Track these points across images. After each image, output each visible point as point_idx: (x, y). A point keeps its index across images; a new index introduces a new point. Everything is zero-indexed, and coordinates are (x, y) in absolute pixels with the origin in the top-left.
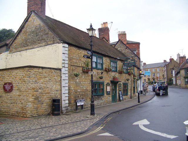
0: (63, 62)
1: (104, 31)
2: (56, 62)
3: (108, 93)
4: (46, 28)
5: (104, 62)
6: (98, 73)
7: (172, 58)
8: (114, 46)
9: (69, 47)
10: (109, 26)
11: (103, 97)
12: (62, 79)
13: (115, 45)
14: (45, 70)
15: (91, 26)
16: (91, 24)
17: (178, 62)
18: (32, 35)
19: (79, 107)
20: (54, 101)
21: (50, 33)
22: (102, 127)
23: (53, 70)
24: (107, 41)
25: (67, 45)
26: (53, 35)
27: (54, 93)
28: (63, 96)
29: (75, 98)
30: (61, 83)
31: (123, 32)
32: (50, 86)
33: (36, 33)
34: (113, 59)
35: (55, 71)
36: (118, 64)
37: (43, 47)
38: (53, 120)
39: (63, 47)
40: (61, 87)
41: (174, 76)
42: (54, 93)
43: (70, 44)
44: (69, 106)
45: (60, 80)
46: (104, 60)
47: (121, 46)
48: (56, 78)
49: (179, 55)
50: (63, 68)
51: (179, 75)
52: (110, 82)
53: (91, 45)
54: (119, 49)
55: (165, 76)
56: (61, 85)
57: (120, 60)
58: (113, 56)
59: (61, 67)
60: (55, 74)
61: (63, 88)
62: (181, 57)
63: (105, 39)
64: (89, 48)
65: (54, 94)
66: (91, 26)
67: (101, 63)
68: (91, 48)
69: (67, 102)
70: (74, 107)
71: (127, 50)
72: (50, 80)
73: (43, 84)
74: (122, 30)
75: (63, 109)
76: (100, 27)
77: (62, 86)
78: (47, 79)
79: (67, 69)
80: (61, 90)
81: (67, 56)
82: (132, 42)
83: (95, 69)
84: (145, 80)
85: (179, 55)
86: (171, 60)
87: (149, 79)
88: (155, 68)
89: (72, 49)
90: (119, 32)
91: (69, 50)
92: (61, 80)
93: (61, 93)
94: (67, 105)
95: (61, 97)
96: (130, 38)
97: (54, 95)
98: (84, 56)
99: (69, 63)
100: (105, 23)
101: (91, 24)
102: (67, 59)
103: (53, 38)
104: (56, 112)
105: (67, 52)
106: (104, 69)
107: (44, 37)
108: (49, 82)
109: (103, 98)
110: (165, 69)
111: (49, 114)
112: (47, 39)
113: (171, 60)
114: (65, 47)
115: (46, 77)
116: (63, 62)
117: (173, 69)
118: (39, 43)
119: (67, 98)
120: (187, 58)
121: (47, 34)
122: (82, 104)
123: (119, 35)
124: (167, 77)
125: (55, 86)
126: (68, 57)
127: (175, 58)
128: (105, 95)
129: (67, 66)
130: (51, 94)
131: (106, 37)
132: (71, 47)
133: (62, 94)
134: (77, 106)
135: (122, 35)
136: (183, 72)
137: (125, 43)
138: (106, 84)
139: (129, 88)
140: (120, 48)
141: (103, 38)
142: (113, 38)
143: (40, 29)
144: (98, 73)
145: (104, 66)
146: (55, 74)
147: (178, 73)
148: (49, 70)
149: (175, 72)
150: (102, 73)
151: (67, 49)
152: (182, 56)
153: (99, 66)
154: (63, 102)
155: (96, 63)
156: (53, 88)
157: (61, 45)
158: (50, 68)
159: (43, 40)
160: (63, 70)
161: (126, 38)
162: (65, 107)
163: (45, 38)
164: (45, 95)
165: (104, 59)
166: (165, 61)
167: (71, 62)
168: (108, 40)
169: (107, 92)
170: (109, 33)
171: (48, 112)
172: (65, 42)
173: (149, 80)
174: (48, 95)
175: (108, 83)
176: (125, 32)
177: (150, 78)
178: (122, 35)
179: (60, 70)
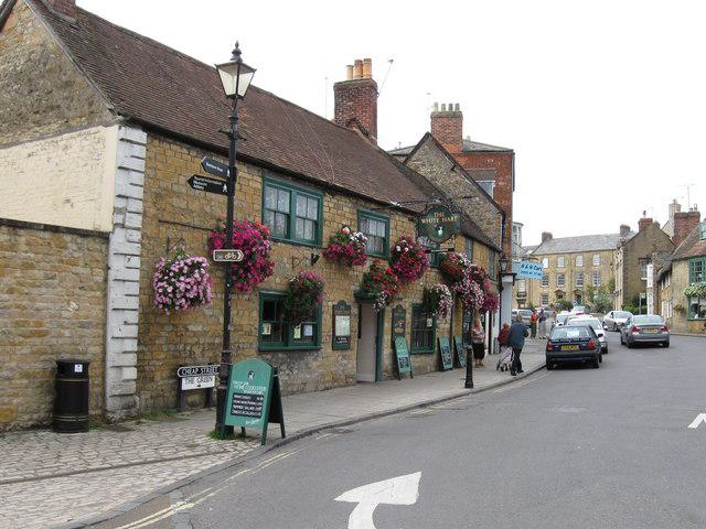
0: (121, 203)
1: (357, 94)
2: (93, 203)
3: (340, 344)
4: (68, 59)
5: (326, 215)
6: (293, 258)
7: (648, 216)
8: (402, 159)
9: (156, 142)
10: (377, 74)
11: (315, 359)
12: (112, 274)
13: (408, 157)
14: (24, 237)
15: (237, 53)
16: (237, 45)
17: (671, 234)
18: (15, 87)
19: (191, 399)
20: (64, 368)
21: (79, 79)
22: (191, 505)
23: (67, 238)
24: (367, 135)
25: (139, 135)
26: (90, 91)
27: (67, 333)
28: (113, 348)
29: (175, 357)
30: (105, 296)
31: (451, 106)
32: (50, 305)
33: (29, 80)
34: (373, 206)
35: (79, 240)
36: (392, 226)
37: (49, 140)
38: (73, 449)
39: (122, 140)
40: (105, 312)
41: (650, 283)
42: (67, 333)
43: (154, 131)
44: (138, 393)
45: (100, 279)
46: (325, 209)
47: (433, 159)
48: (80, 270)
49: (675, 205)
50: (118, 230)
51: (668, 283)
52: (353, 299)
53: (231, 136)
54: (423, 171)
55: (619, 286)
56: (105, 303)
57: (405, 212)
58: (371, 194)
59: (106, 227)
60: (76, 255)
61: (111, 314)
62: (684, 214)
63: (360, 128)
64: (225, 143)
65: (68, 341)
66: (237, 53)
67: (287, 211)
68: (233, 145)
69: (131, 373)
70: (171, 397)
71: (457, 177)
72: (53, 278)
73: (15, 296)
74: (446, 99)
75: (111, 404)
76: (343, 77)
77: (111, 306)
78: (38, 274)
79: (137, 236)
80: (105, 325)
81: (138, 178)
82: (490, 149)
83: (285, 242)
84: (545, 297)
85: (675, 205)
86: (646, 224)
87: (560, 295)
88: (695, 260)
89: (169, 153)
90: (436, 105)
91: (148, 159)
92: (106, 280)
93: (104, 337)
94: (133, 387)
95: (104, 352)
96: (478, 131)
97: (66, 342)
98: (191, 181)
99: (153, 211)
100: (362, 64)
101: (237, 45)
102: (138, 192)
103: (91, 104)
104: (70, 418)
105: (140, 165)
106: (325, 245)
107: (59, 97)
108: (47, 286)
109: (315, 364)
110: (620, 257)
111: (37, 427)
112: (68, 108)
113: (646, 224)
114: (131, 142)
115: (32, 267)
116: (121, 203)
117: (648, 260)
118: (38, 123)
119: (132, 359)
120: (702, 220)
121: (68, 84)
122: (204, 385)
123: (436, 118)
124: (625, 288)
125: (74, 305)
126: (146, 188)
127: (663, 218)
128: (326, 348)
129: (136, 221)
130: (54, 341)
131: (365, 121)
132: (166, 145)
133: (109, 338)
134: (180, 394)
135: (449, 120)
136: (681, 272)
137: (450, 148)
138: (330, 304)
139: (442, 326)
140: (432, 168)
141: (349, 124)
142: (399, 128)
143: (45, 64)
144: (293, 258)
145: (327, 232)
146: (76, 255)
147: (664, 276)
148: (47, 235)
149: (656, 271)
150: (314, 260)
151: (141, 151)
152: (687, 211)
153: (304, 232)
154: (111, 375)
155: (288, 217)
156: (65, 314)
157: (113, 133)
158: (55, 229)
159: (52, 108)
160: (118, 240)
161: (459, 128)
162: (121, 396)
163: (59, 102)
164: (20, 344)
165: (329, 202)
166: (625, 229)
167: (162, 204)
168: (371, 132)
169: (335, 338)
170: (376, 104)
171: (35, 416)
172: (132, 122)
173: (560, 297)
174: (37, 340)
175: (342, 303)
176: (457, 105)
177: (566, 289)
178: (449, 120)
179: (104, 237)
